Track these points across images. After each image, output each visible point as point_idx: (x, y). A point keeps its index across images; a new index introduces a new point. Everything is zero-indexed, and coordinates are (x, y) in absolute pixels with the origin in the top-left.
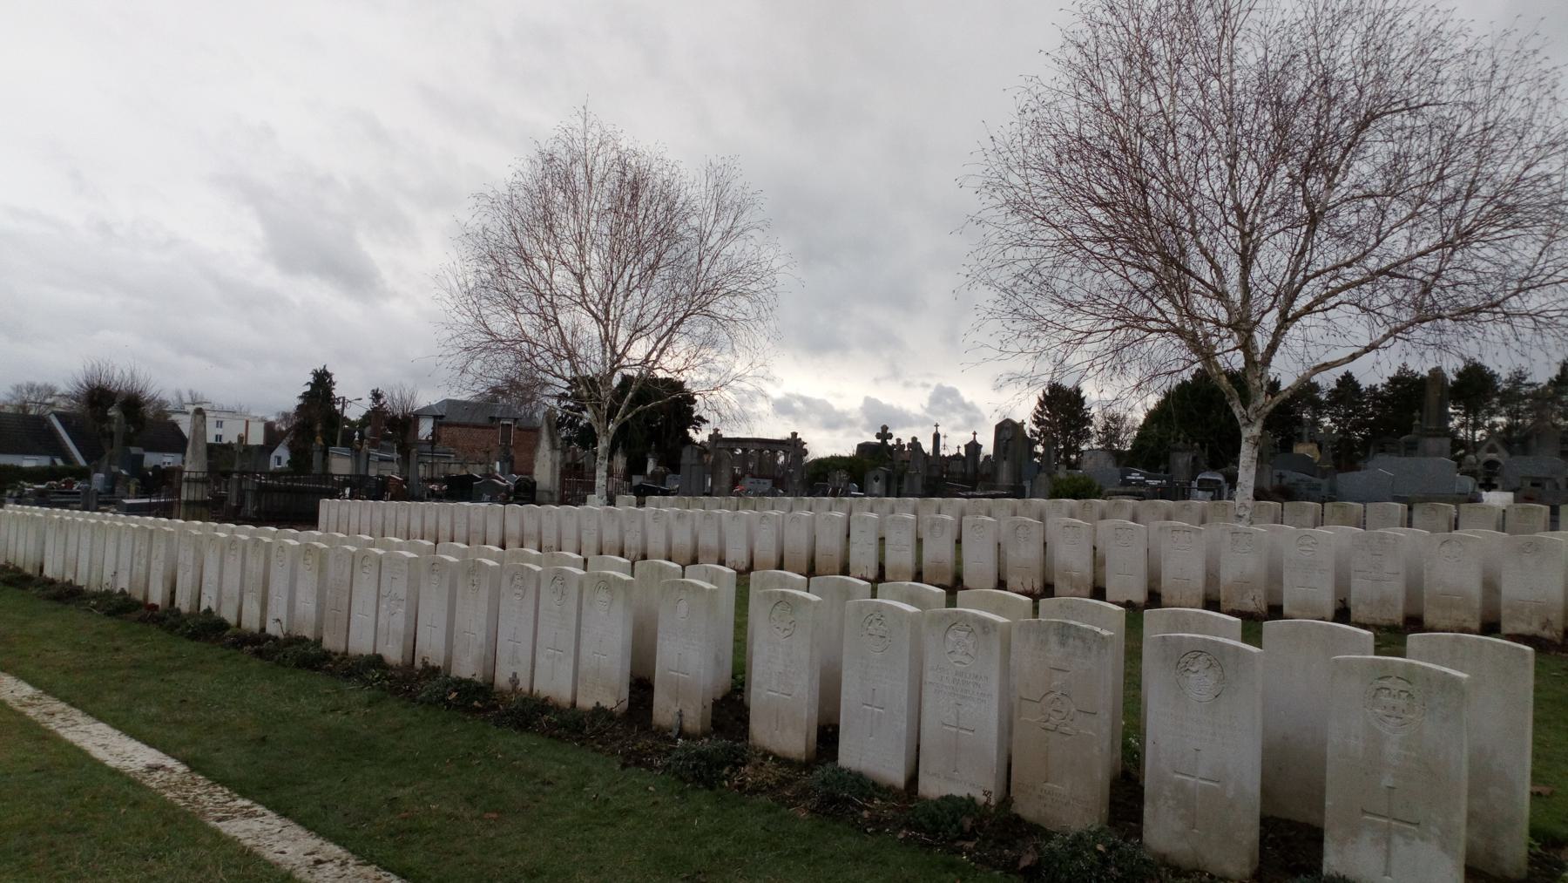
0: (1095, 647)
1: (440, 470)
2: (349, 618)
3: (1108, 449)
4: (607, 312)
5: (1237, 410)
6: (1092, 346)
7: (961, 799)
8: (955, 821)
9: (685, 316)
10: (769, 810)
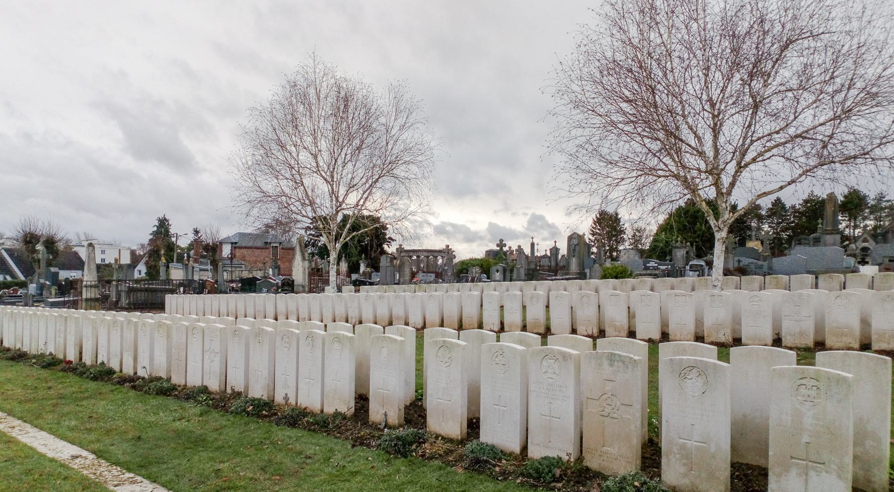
0: (630, 366)
1: (236, 275)
4: (332, 177)
5: (712, 222)
6: (624, 187)
7: (554, 458)
8: (550, 471)
9: (379, 178)
10: (440, 468)
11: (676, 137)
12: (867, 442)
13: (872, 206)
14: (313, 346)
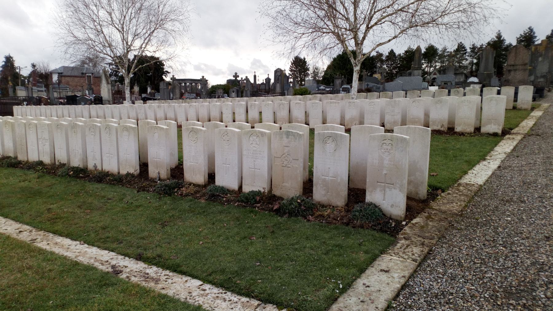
0: (298, 138)
1: (63, 94)
4: (123, 28)
5: (352, 60)
6: (305, 39)
7: (256, 191)
8: (254, 198)
9: (155, 29)
10: (191, 201)
11: (333, 8)
13: (440, 54)
14: (110, 134)
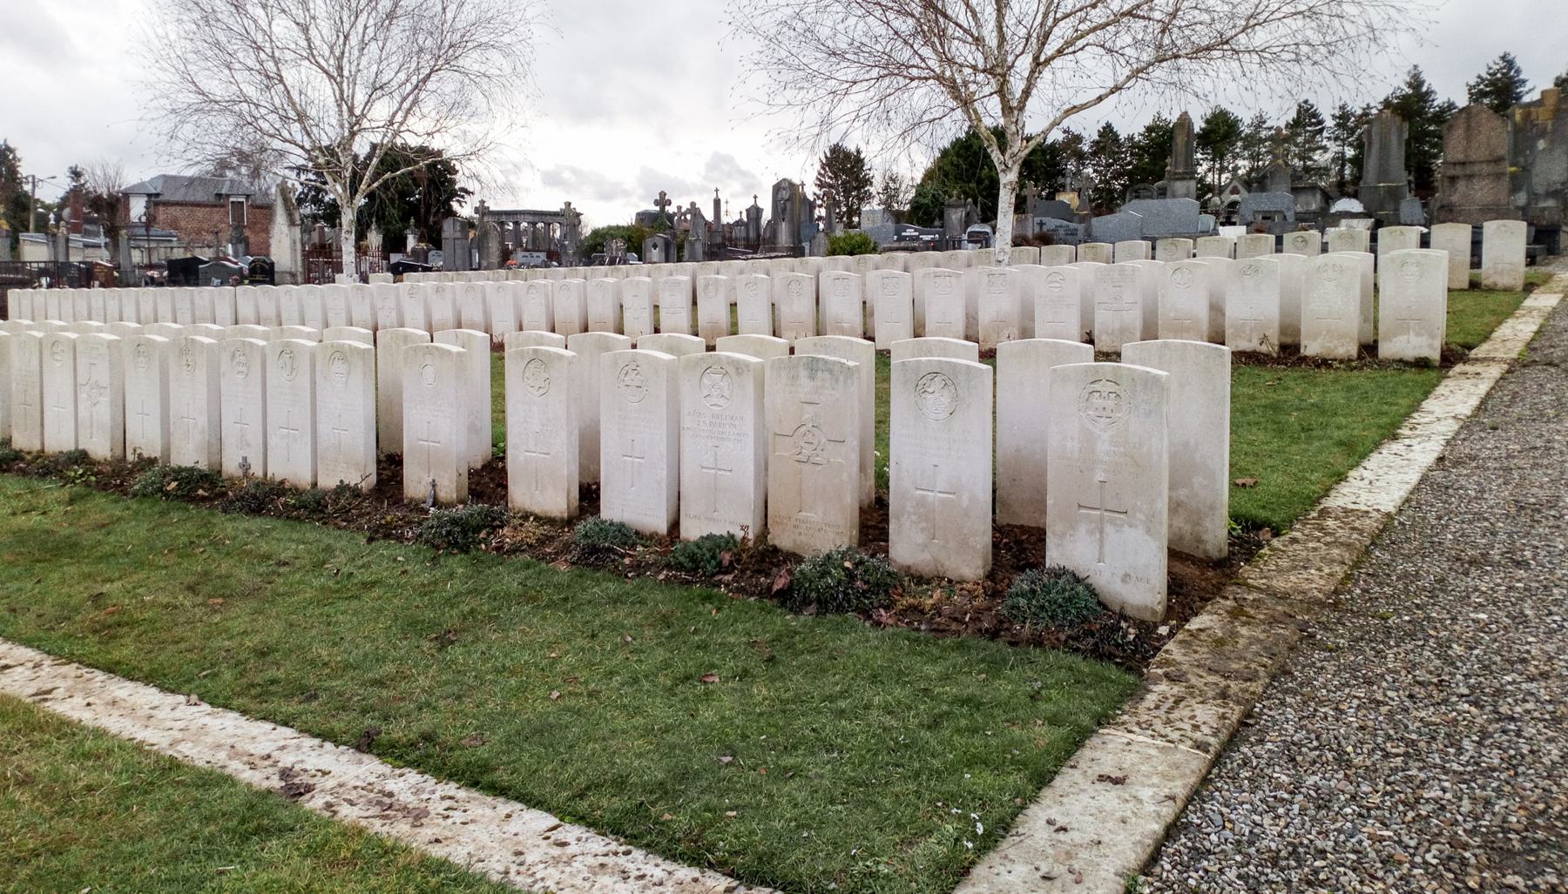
0: (841, 378)
1: (160, 255)
2: (42, 413)
3: (888, 205)
4: (340, 68)
5: (995, 155)
6: (858, 96)
7: (722, 537)
8: (713, 557)
10: (528, 566)
12: (1194, 480)
14: (293, 369)
